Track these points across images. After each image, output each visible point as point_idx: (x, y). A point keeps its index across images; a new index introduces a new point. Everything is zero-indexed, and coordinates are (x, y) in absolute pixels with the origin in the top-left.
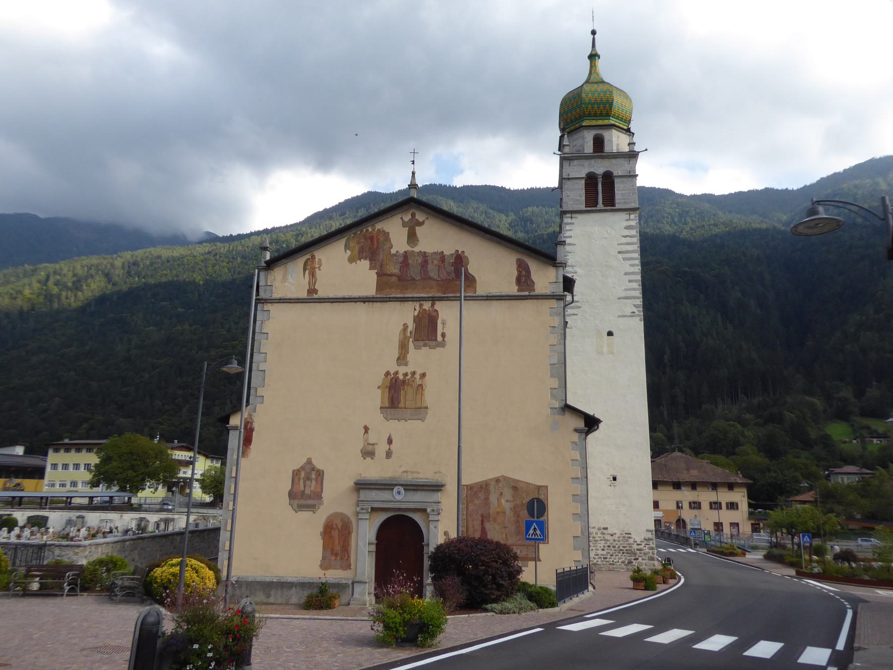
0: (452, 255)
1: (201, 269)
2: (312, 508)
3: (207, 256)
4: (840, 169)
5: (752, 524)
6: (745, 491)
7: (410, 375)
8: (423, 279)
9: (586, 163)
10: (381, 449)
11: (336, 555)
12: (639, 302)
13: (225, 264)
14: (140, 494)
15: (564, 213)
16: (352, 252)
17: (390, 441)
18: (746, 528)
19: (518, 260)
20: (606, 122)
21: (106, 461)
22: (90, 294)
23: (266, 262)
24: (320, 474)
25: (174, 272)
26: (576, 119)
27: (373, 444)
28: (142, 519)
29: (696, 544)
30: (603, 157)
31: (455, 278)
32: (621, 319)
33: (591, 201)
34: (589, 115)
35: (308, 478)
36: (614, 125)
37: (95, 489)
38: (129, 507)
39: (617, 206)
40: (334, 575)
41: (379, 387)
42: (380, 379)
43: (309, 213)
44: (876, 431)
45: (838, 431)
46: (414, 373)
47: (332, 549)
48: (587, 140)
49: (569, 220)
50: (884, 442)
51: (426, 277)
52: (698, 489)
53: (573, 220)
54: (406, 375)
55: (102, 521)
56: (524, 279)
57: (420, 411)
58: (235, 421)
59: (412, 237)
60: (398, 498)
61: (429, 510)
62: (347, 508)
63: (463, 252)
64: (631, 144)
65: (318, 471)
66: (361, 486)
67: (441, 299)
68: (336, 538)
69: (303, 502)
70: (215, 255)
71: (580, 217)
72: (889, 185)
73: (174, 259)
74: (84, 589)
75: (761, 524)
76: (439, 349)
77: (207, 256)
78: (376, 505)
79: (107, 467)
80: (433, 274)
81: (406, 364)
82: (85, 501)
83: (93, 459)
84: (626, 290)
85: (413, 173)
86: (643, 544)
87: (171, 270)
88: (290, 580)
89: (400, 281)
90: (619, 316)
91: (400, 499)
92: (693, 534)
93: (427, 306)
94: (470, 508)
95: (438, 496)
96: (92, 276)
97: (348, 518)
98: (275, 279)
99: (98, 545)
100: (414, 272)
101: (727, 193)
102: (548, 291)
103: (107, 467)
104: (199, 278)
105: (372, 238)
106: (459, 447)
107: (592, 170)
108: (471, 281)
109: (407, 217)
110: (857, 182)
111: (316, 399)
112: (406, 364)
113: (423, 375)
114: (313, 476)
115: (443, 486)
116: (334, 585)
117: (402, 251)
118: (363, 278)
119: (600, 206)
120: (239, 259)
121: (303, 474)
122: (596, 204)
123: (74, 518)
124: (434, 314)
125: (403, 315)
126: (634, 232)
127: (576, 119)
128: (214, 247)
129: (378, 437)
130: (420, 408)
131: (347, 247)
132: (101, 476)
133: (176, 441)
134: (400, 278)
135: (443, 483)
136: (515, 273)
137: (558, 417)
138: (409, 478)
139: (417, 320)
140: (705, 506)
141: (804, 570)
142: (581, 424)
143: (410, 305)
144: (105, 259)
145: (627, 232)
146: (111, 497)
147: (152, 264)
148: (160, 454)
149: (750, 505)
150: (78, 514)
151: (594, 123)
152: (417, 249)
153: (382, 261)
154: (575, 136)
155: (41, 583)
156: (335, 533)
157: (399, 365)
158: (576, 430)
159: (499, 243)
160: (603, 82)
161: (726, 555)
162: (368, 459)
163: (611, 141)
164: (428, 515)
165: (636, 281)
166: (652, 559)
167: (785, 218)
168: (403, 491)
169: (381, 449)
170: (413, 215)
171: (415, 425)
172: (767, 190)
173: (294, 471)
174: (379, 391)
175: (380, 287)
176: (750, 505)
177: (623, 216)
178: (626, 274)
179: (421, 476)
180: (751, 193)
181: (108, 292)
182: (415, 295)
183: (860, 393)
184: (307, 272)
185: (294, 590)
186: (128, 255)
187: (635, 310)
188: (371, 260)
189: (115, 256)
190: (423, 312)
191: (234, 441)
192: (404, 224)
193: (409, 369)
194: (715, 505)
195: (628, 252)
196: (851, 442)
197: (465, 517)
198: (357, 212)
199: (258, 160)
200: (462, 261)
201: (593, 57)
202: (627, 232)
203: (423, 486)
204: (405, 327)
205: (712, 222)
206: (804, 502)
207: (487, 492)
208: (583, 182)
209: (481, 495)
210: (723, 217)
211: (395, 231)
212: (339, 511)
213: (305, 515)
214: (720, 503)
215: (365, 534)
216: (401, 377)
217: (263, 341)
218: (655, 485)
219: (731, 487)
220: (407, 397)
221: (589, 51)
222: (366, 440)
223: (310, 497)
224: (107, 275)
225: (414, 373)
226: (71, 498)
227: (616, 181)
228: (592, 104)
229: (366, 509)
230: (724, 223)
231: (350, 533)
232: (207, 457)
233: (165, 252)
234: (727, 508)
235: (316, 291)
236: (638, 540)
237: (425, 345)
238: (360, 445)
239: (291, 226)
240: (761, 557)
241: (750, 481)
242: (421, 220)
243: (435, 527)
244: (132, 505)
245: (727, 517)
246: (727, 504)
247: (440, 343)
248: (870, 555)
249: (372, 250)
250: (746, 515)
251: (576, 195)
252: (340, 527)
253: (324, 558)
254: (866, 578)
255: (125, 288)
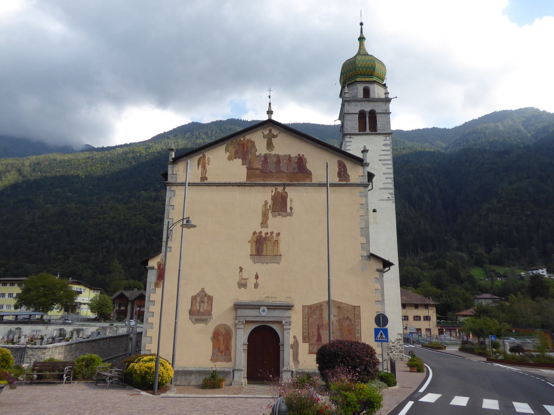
0: (296, 157)
1: (83, 168)
2: (205, 321)
3: (87, 160)
4: (476, 117)
5: (439, 329)
6: (435, 309)
7: (269, 234)
8: (277, 172)
9: (359, 104)
10: (251, 282)
11: (222, 352)
12: (392, 191)
13: (99, 165)
14: (50, 313)
15: (345, 135)
16: (230, 153)
17: (257, 277)
18: (435, 332)
19: (339, 161)
20: (371, 79)
21: (26, 291)
22: (7, 182)
23: (173, 159)
24: (210, 299)
25: (65, 170)
26: (352, 77)
27: (246, 279)
28: (61, 330)
29: (413, 342)
30: (369, 101)
31: (299, 172)
32: (381, 202)
33: (362, 128)
34: (361, 75)
35: (202, 301)
36: (376, 81)
37: (19, 310)
38: (41, 322)
39: (378, 132)
40: (220, 366)
41: (249, 242)
42: (250, 236)
43: (154, 135)
44: (499, 273)
45: (477, 273)
46: (272, 233)
47: (219, 348)
48: (359, 89)
49: (349, 140)
50: (504, 280)
51: (279, 171)
52: (407, 308)
53: (351, 140)
54: (267, 234)
55: (33, 331)
56: (342, 173)
57: (277, 257)
58: (153, 263)
59: (270, 145)
60: (263, 314)
61: (284, 322)
62: (229, 321)
63: (303, 155)
64: (387, 93)
65: (209, 296)
66: (238, 306)
67: (289, 185)
68: (222, 340)
69: (198, 317)
70: (92, 159)
71: (356, 137)
72: (504, 127)
73: (65, 161)
74: (75, 379)
75: (444, 330)
76: (288, 218)
77: (87, 160)
78: (248, 319)
79: (27, 296)
80: (284, 169)
81: (267, 227)
82: (11, 318)
83: (16, 290)
84: (384, 183)
85: (270, 104)
86: (396, 343)
87: (63, 168)
88: (190, 369)
89: (262, 173)
90: (380, 200)
91: (264, 315)
92: (411, 336)
93: (280, 189)
94: (310, 321)
95: (287, 313)
96: (8, 171)
97: (229, 328)
98: (178, 170)
99: (56, 347)
100: (272, 167)
101: (410, 130)
102: (358, 182)
103: (27, 296)
104: (81, 173)
105: (243, 145)
106: (329, 280)
107: (363, 109)
108: (308, 174)
109: (266, 132)
110: (486, 125)
111: (208, 250)
112: (267, 227)
113: (278, 234)
114: (206, 300)
115: (293, 306)
116: (220, 372)
117: (263, 154)
118: (238, 170)
119: (368, 131)
120: (108, 162)
121: (198, 299)
122: (365, 130)
123: (14, 329)
124: (285, 195)
125: (265, 195)
126: (388, 148)
127: (352, 77)
128: (91, 154)
129: (249, 274)
130: (277, 256)
131: (227, 150)
132: (23, 300)
133: (70, 278)
134: (262, 171)
135: (293, 304)
136: (337, 170)
137: (366, 262)
138: (270, 301)
139: (274, 198)
140: (411, 318)
141: (492, 357)
142: (381, 266)
143: (269, 189)
144: (17, 160)
145: (384, 148)
146: (30, 315)
147: (50, 164)
148: (64, 287)
149: (438, 318)
150: (17, 326)
151: (363, 79)
152: (273, 153)
153: (250, 159)
154: (352, 88)
155: (38, 375)
156: (221, 338)
157: (262, 227)
158: (378, 270)
159: (326, 150)
160: (368, 55)
161: (435, 348)
162: (243, 289)
163: (374, 91)
164: (283, 325)
165: (390, 178)
166: (401, 352)
167: (444, 145)
168: (266, 310)
169: (251, 282)
170: (270, 131)
171: (273, 267)
172: (434, 129)
173: (192, 297)
174: (249, 245)
175: (249, 177)
176: (438, 318)
177: (382, 137)
178: (384, 174)
179: (277, 300)
180: (425, 130)
181: (20, 181)
182: (273, 182)
183: (489, 251)
184: (200, 166)
185: (193, 375)
186: (33, 158)
187: (390, 196)
188: (242, 159)
189: (24, 158)
190: (277, 193)
191: (152, 276)
192: (264, 137)
193: (269, 230)
194: (417, 318)
195: (385, 160)
196: (484, 279)
197: (307, 326)
198: (185, 134)
199: (118, 100)
200: (302, 161)
201: (361, 39)
202: (384, 148)
203: (279, 306)
204: (266, 203)
205: (402, 147)
206: (466, 316)
207: (321, 310)
208: (357, 116)
209: (318, 312)
210: (409, 144)
211: (259, 140)
212: (223, 323)
213: (200, 326)
214: (420, 317)
215: (241, 338)
216: (264, 235)
217: (171, 211)
218: (404, 306)
219: (426, 306)
220: (268, 248)
221: (358, 36)
222: (241, 276)
223: (203, 314)
224: (19, 171)
225: (272, 233)
226: (3, 316)
227: (378, 116)
228: (362, 68)
229: (242, 322)
230: (409, 148)
231: (230, 338)
232: (91, 289)
233: (59, 157)
234: (424, 320)
235: (206, 179)
236: (393, 340)
237: (279, 215)
238: (237, 279)
239: (142, 142)
240: (457, 350)
241: (438, 303)
242: (275, 134)
243: (288, 333)
244: (44, 320)
245: (423, 325)
246: (424, 317)
247: (289, 213)
248: (532, 349)
249: (244, 152)
250: (435, 323)
251: (353, 124)
252: (224, 334)
253: (213, 354)
254: (531, 362)
255: (32, 178)
